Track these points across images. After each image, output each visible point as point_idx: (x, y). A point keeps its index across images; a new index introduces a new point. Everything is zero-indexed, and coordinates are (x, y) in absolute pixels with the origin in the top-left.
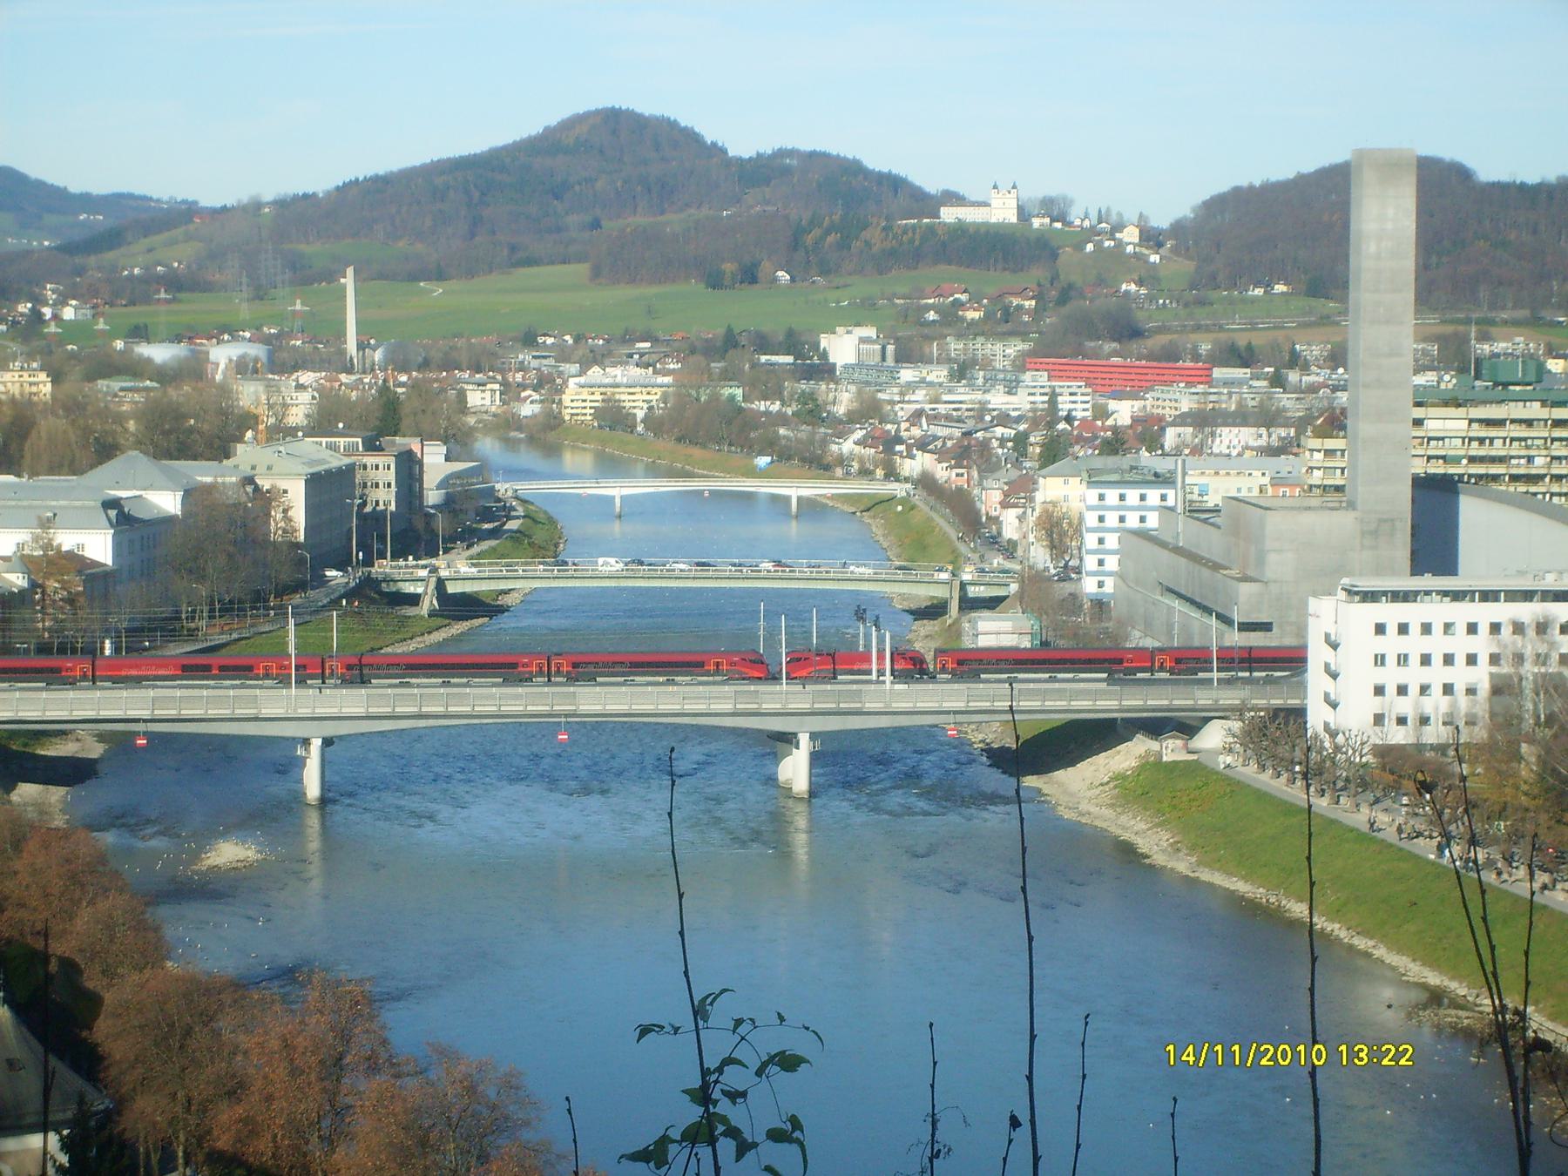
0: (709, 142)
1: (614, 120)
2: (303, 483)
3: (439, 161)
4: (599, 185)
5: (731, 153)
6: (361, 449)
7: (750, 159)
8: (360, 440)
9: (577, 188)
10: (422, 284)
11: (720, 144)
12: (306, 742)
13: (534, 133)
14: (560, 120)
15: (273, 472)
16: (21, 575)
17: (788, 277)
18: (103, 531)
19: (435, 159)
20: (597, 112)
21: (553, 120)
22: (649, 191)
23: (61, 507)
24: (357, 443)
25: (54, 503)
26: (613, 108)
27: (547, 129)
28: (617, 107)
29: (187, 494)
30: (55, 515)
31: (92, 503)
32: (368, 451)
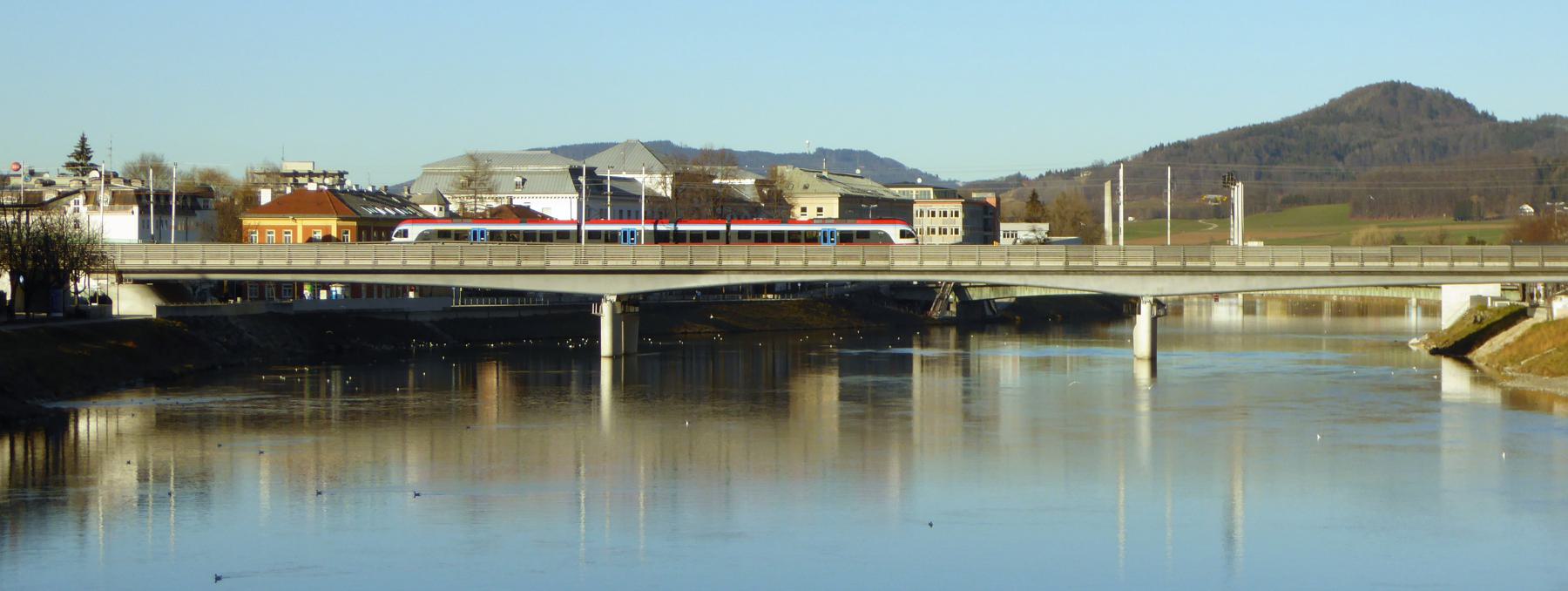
0: (1480, 112)
1: (1393, 92)
2: (837, 201)
3: (1234, 129)
4: (1376, 148)
5: (1499, 119)
6: (932, 197)
7: (1516, 124)
8: (931, 190)
9: (1357, 151)
10: (1200, 221)
11: (1490, 114)
12: (598, 299)
13: (1320, 104)
14: (1344, 93)
15: (808, 190)
16: (437, 207)
17: (1532, 210)
18: (568, 195)
19: (1232, 128)
20: (1378, 86)
21: (1338, 93)
22: (1423, 152)
23: (529, 173)
24: (929, 192)
25: (524, 169)
26: (1392, 82)
27: (1332, 101)
28: (1396, 81)
29: (678, 177)
30: (524, 181)
31: (560, 168)
32: (938, 198)
